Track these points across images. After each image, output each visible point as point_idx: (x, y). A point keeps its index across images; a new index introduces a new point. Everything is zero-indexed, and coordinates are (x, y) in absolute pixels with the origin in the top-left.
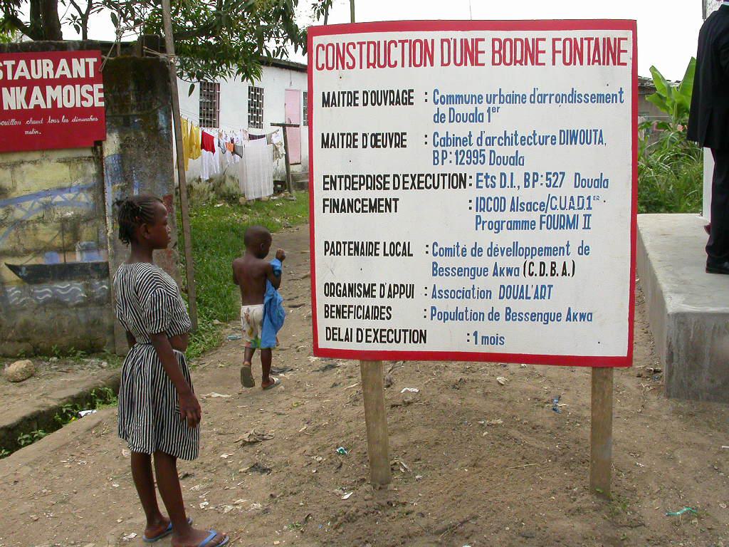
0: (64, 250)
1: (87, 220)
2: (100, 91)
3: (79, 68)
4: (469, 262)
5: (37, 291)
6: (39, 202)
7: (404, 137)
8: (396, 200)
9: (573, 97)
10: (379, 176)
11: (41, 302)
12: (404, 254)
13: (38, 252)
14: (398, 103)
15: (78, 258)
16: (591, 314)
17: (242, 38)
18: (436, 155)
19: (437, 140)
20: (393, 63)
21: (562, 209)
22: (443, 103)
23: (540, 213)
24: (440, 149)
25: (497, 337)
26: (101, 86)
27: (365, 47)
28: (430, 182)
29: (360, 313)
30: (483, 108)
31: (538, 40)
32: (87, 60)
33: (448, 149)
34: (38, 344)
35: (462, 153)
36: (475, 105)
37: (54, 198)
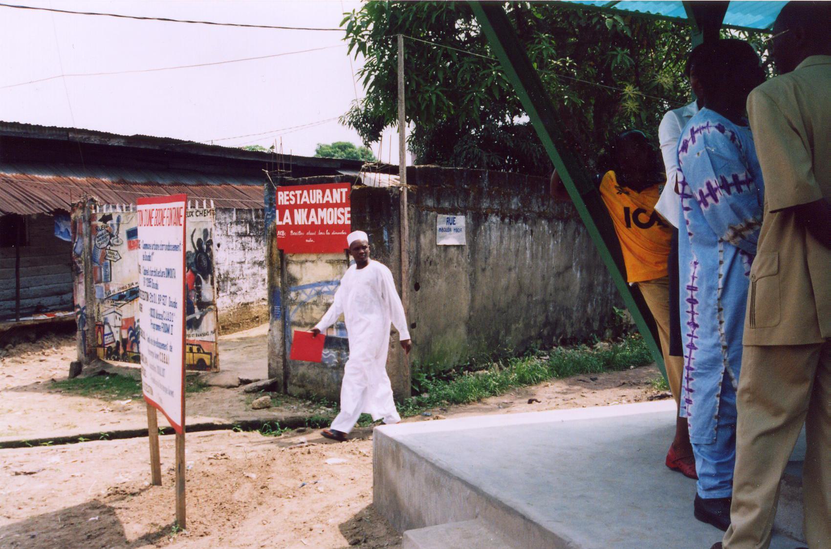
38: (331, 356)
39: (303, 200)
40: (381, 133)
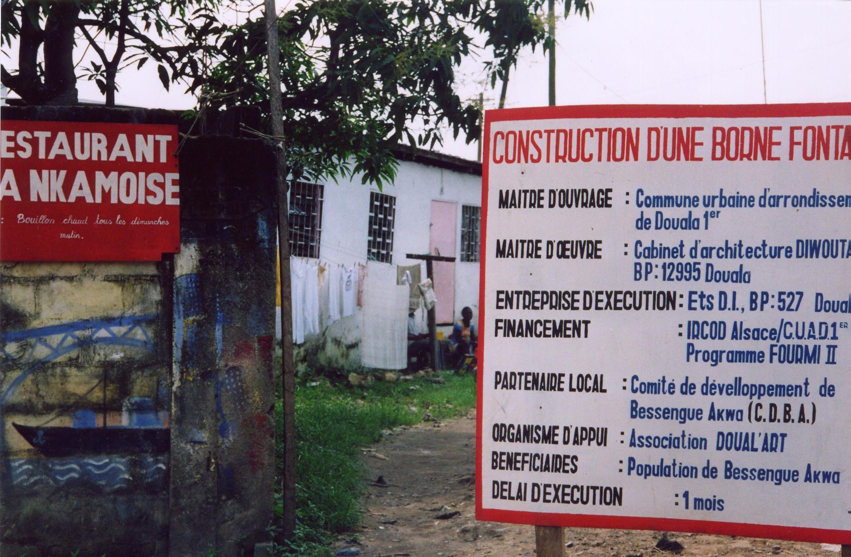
0: (104, 408)
1: (143, 366)
2: (174, 182)
3: (145, 148)
4: (678, 401)
5: (58, 468)
6: (73, 337)
7: (599, 246)
8: (587, 323)
9: (815, 200)
10: (567, 293)
11: (62, 484)
12: (596, 389)
13: (64, 409)
14: (592, 204)
15: (125, 421)
16: (838, 474)
17: (366, 111)
18: (638, 269)
19: (640, 249)
20: (587, 156)
21: (799, 338)
22: (648, 206)
23: (769, 342)
24: (643, 261)
25: (715, 500)
26: (176, 176)
27: (553, 136)
28: (630, 301)
29: (538, 463)
30: (699, 212)
31: (772, 128)
32: (158, 137)
33: (654, 261)
34: (51, 547)
35: (671, 266)
36: (687, 209)
37: (95, 332)
38: (113, 468)
39: (55, 151)
40: (262, 16)
